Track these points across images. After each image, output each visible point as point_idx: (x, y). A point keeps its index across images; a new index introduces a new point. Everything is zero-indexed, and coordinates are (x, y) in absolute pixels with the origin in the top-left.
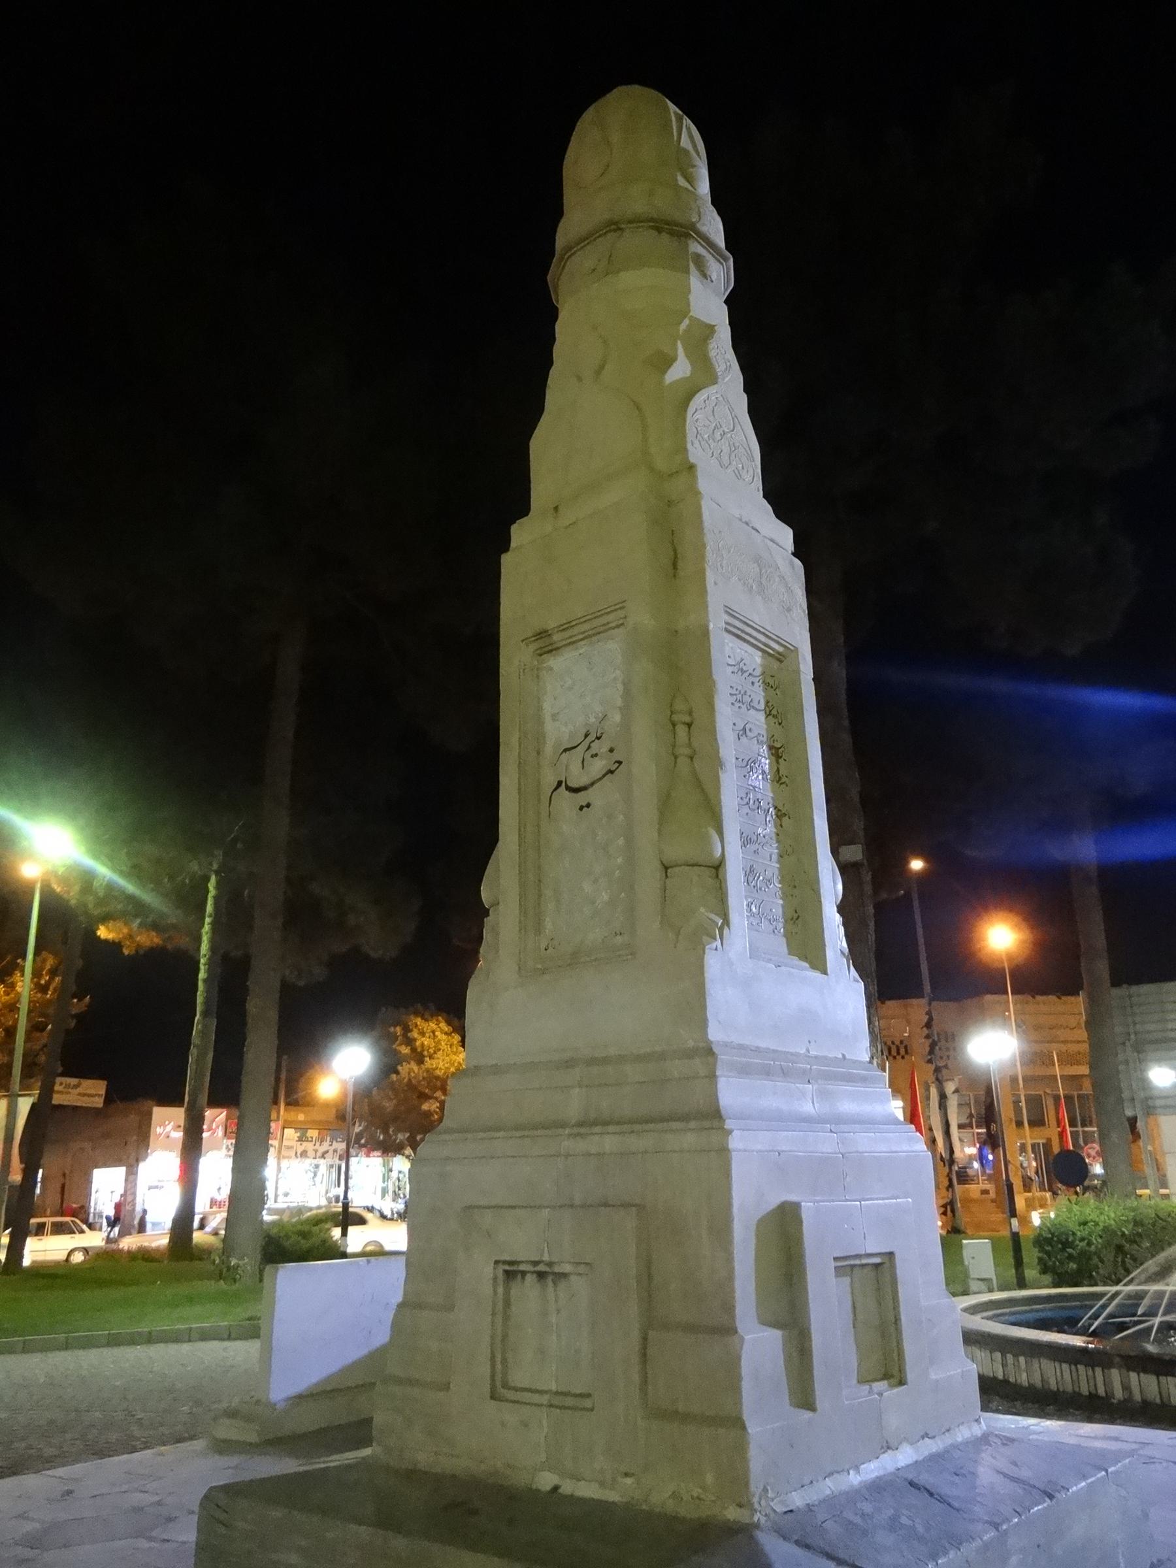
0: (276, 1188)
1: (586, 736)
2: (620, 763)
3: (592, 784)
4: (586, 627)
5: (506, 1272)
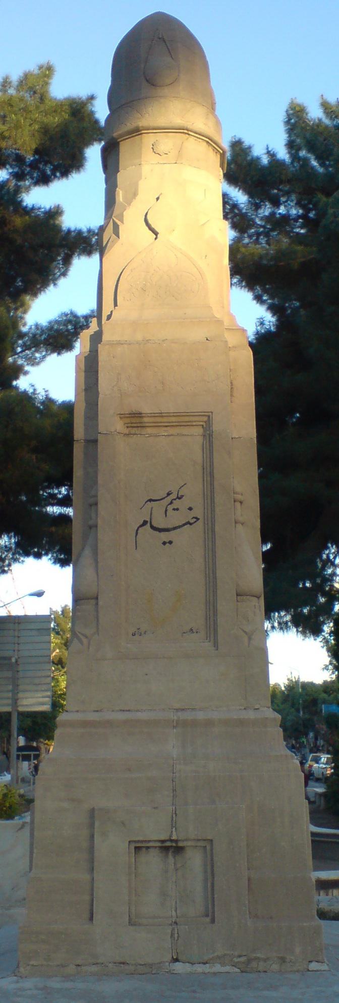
1: (168, 494)
2: (198, 519)
3: (175, 528)
4: (173, 419)
5: (136, 848)
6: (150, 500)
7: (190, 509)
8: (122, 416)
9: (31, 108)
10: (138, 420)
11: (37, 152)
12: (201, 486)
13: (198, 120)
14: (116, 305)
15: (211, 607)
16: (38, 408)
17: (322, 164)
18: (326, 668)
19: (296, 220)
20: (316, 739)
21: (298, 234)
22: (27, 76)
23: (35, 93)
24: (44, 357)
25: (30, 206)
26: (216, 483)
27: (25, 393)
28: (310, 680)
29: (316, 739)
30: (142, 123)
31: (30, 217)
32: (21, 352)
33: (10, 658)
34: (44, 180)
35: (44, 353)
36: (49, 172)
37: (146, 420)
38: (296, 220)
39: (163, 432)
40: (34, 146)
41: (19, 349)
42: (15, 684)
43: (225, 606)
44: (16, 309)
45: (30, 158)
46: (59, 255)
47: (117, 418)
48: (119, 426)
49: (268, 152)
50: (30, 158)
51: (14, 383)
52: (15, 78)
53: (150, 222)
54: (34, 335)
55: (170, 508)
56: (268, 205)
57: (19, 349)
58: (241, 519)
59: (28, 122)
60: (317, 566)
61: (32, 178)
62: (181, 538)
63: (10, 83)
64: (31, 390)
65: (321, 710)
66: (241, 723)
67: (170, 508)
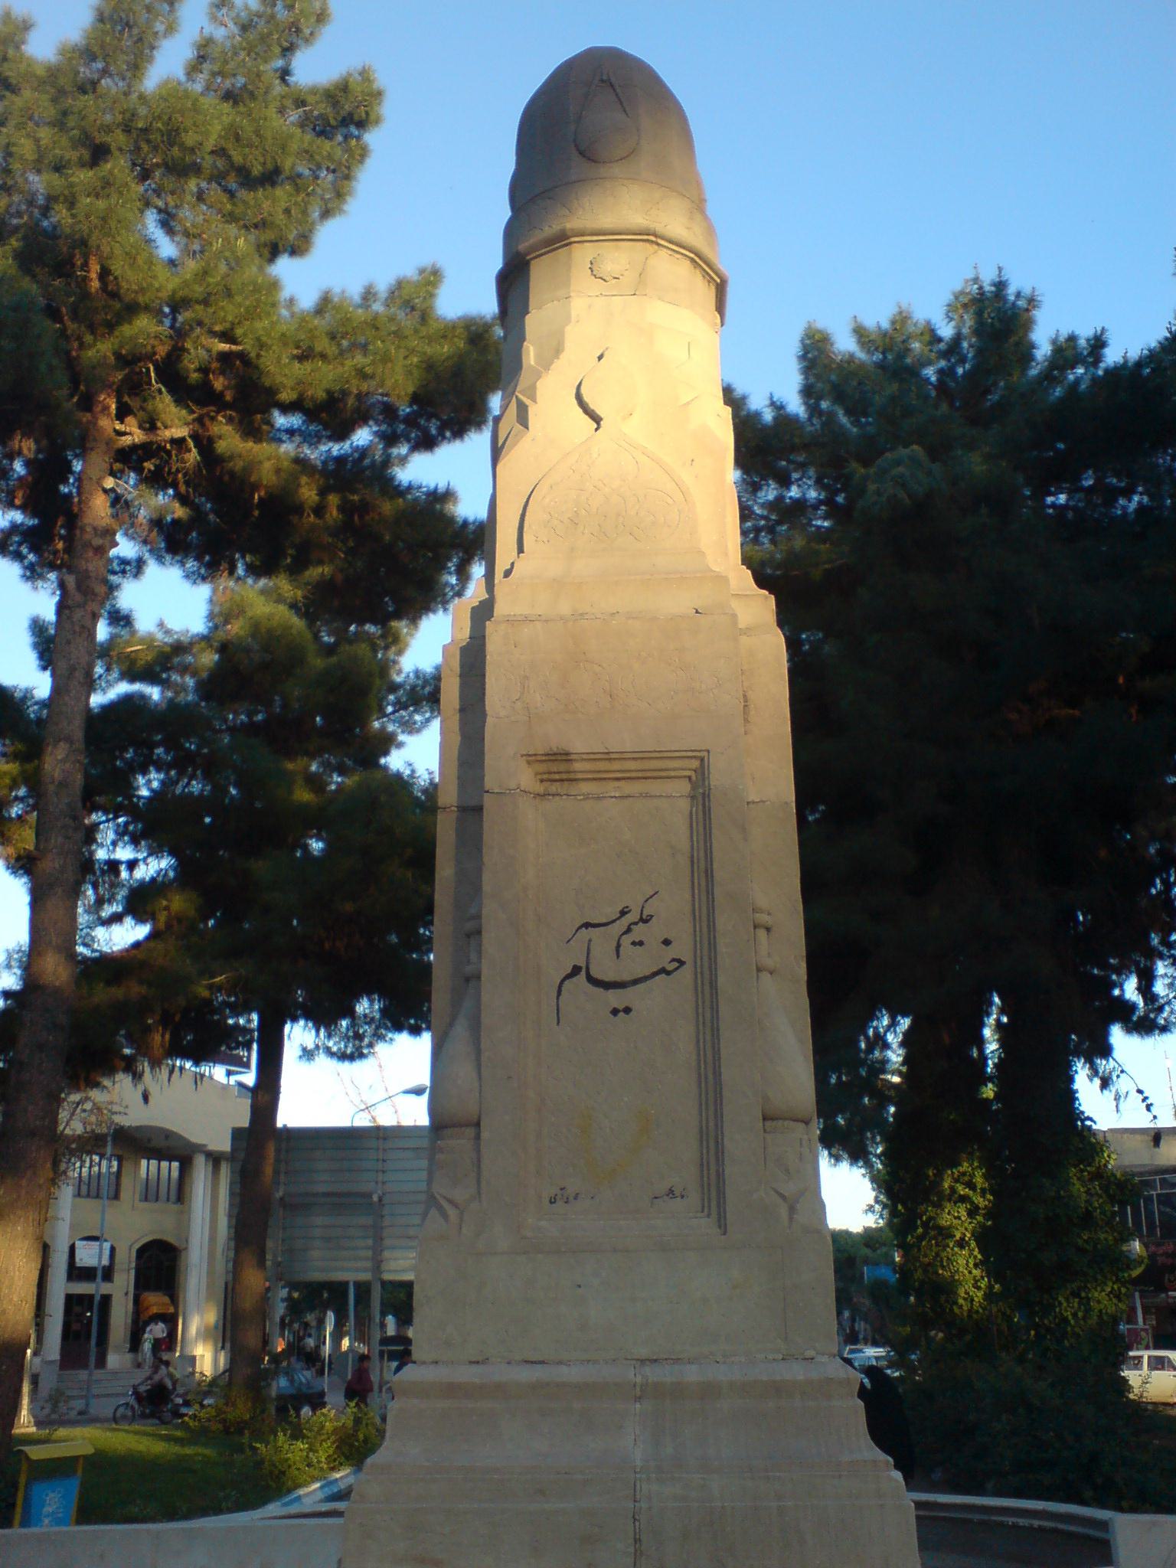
0: (275, 1518)
1: (623, 913)
2: (682, 963)
3: (636, 982)
4: (632, 765)
6: (587, 925)
7: (667, 942)
8: (531, 759)
9: (407, 332)
10: (562, 767)
11: (415, 399)
12: (688, 896)
13: (675, 222)
14: (521, 550)
15: (712, 1145)
16: (417, 798)
17: (856, 423)
18: (871, 1209)
19: (816, 507)
20: (853, 1320)
21: (819, 528)
22: (400, 284)
23: (413, 309)
24: (428, 720)
25: (405, 483)
26: (717, 891)
27: (398, 776)
28: (844, 1228)
29: (853, 1320)
30: (572, 224)
31: (405, 499)
32: (393, 713)
33: (369, 1195)
34: (427, 443)
35: (428, 715)
36: (434, 431)
37: (577, 766)
38: (816, 507)
39: (611, 789)
40: (411, 389)
41: (390, 709)
42: (378, 1237)
43: (741, 1140)
44: (387, 648)
45: (405, 409)
46: (450, 559)
47: (522, 762)
48: (526, 778)
49: (773, 404)
50: (405, 409)
51: (383, 761)
52: (382, 286)
53: (586, 398)
54: (413, 688)
55: (626, 941)
56: (773, 484)
57: (390, 709)
58: (769, 963)
59: (402, 352)
60: (859, 1049)
61: (408, 441)
62: (647, 1000)
63: (375, 294)
64: (408, 772)
65: (862, 1277)
66: (778, 1389)
67: (626, 941)
